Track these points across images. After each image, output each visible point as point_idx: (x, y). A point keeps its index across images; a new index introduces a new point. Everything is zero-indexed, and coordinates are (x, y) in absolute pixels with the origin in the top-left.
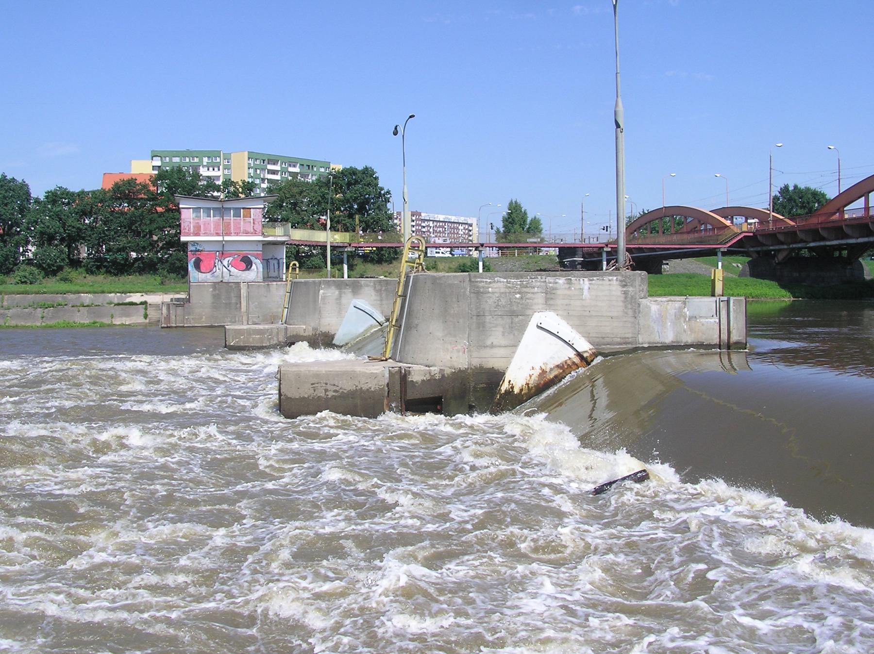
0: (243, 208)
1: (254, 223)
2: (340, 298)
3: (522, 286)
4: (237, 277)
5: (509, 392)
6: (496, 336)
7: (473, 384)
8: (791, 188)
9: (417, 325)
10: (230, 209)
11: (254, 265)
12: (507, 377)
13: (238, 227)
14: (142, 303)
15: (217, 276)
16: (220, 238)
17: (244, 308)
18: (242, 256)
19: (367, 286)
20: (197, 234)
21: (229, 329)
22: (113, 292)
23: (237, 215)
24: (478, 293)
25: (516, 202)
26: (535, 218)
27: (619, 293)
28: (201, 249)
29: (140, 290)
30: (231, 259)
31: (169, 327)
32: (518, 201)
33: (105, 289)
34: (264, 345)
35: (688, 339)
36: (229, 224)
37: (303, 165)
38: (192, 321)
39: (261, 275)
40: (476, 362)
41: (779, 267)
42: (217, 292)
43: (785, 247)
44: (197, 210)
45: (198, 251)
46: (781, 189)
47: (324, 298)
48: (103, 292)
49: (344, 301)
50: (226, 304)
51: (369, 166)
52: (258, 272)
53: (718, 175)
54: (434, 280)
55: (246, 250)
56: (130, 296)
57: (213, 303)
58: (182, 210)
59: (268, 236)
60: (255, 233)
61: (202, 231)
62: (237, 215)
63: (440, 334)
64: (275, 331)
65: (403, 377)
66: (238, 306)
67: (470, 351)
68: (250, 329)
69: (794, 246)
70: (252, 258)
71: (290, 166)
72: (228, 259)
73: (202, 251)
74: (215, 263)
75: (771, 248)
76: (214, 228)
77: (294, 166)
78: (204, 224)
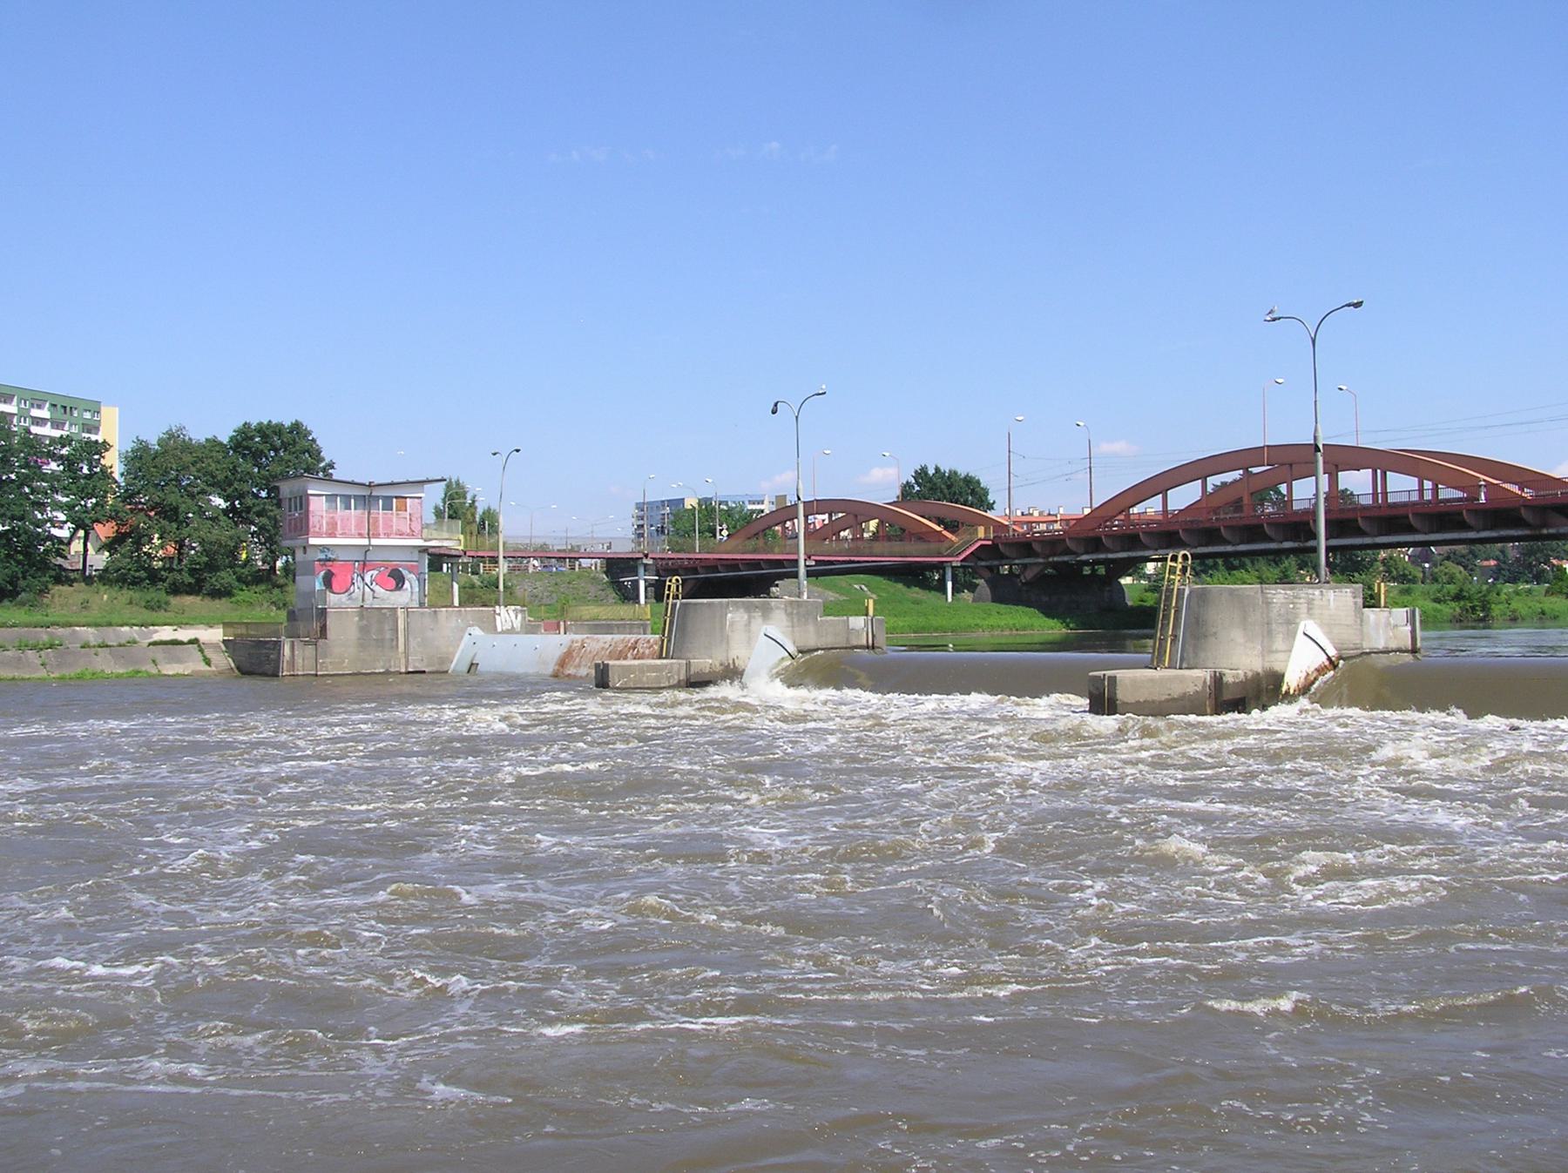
0: (396, 497)
1: (410, 520)
2: (749, 623)
3: (1295, 597)
4: (383, 600)
5: (1287, 693)
6: (1279, 644)
7: (1265, 686)
8: (931, 472)
9: (1215, 633)
10: (378, 498)
11: (406, 582)
12: (1286, 679)
13: (388, 525)
14: (191, 642)
15: (357, 599)
16: (365, 542)
18: (390, 568)
19: (778, 608)
20: (332, 535)
21: (613, 666)
22: (127, 625)
23: (387, 507)
24: (1268, 603)
25: (458, 483)
26: (489, 509)
27: (1352, 604)
28: (333, 557)
29: (168, 621)
30: (375, 572)
33: (114, 621)
34: (662, 685)
35: (1393, 645)
36: (376, 520)
37: (55, 406)
38: (330, 667)
40: (1267, 665)
41: (1024, 588)
42: (365, 622)
43: (1041, 560)
45: (329, 560)
46: (916, 472)
47: (732, 624)
48: (110, 625)
49: (754, 626)
51: (300, 420)
52: (412, 593)
53: (887, 454)
54: (1231, 592)
55: (396, 559)
56: (156, 631)
57: (359, 639)
58: (311, 498)
59: (430, 540)
60: (412, 535)
61: (339, 531)
62: (387, 507)
63: (1241, 640)
64: (676, 668)
65: (1218, 680)
66: (395, 643)
67: (1263, 656)
69: (1055, 559)
70: (405, 572)
71: (32, 406)
72: (371, 572)
73: (334, 560)
74: (353, 579)
75: (1084, 557)
76: (357, 526)
77: (39, 407)
78: (342, 520)
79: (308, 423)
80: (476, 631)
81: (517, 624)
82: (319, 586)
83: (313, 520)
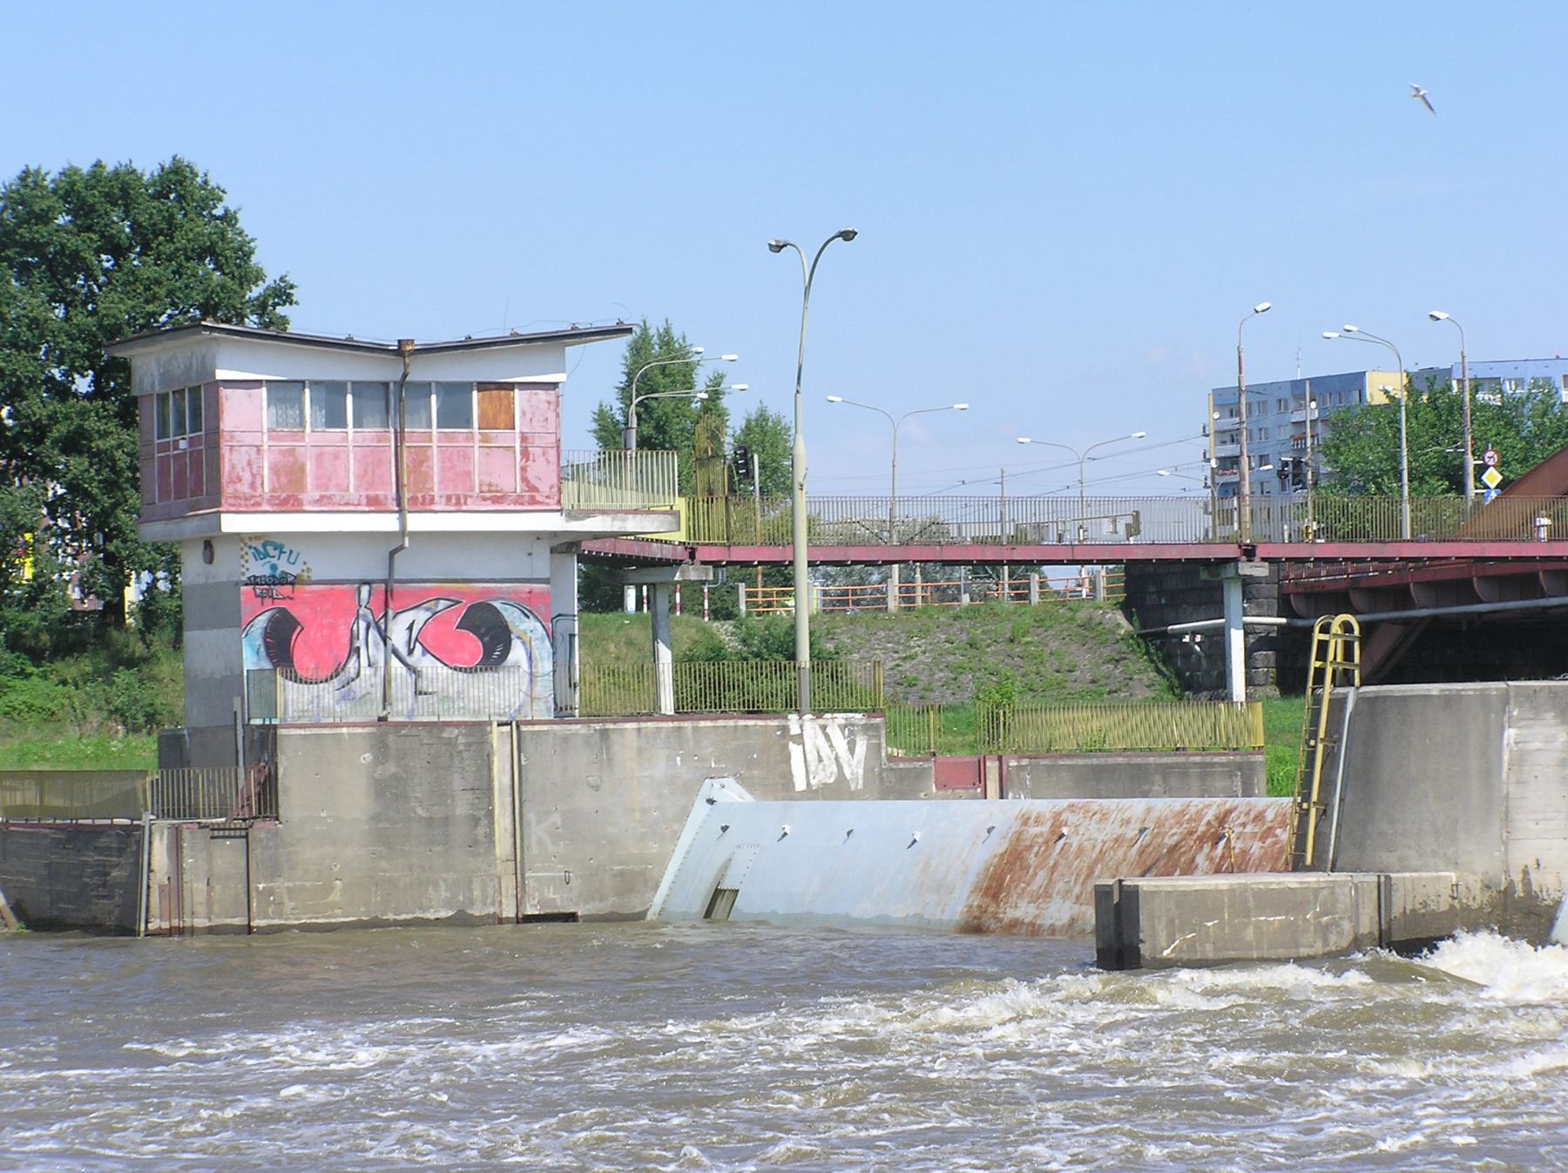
1: (525, 454)
16: (387, 523)
17: (503, 846)
20: (288, 503)
21: (1153, 894)
23: (455, 415)
25: (667, 341)
28: (294, 570)
30: (420, 616)
31: (180, 931)
32: (676, 334)
36: (422, 457)
39: (544, 688)
42: (392, 768)
44: (284, 391)
47: (1520, 760)
50: (430, 821)
57: (375, 818)
59: (588, 514)
60: (530, 499)
61: (311, 492)
66: (481, 830)
68: (1244, 889)
70: (511, 615)
74: (353, 637)
79: (211, 166)
80: (731, 792)
81: (855, 768)
82: (252, 658)
83: (232, 460)
